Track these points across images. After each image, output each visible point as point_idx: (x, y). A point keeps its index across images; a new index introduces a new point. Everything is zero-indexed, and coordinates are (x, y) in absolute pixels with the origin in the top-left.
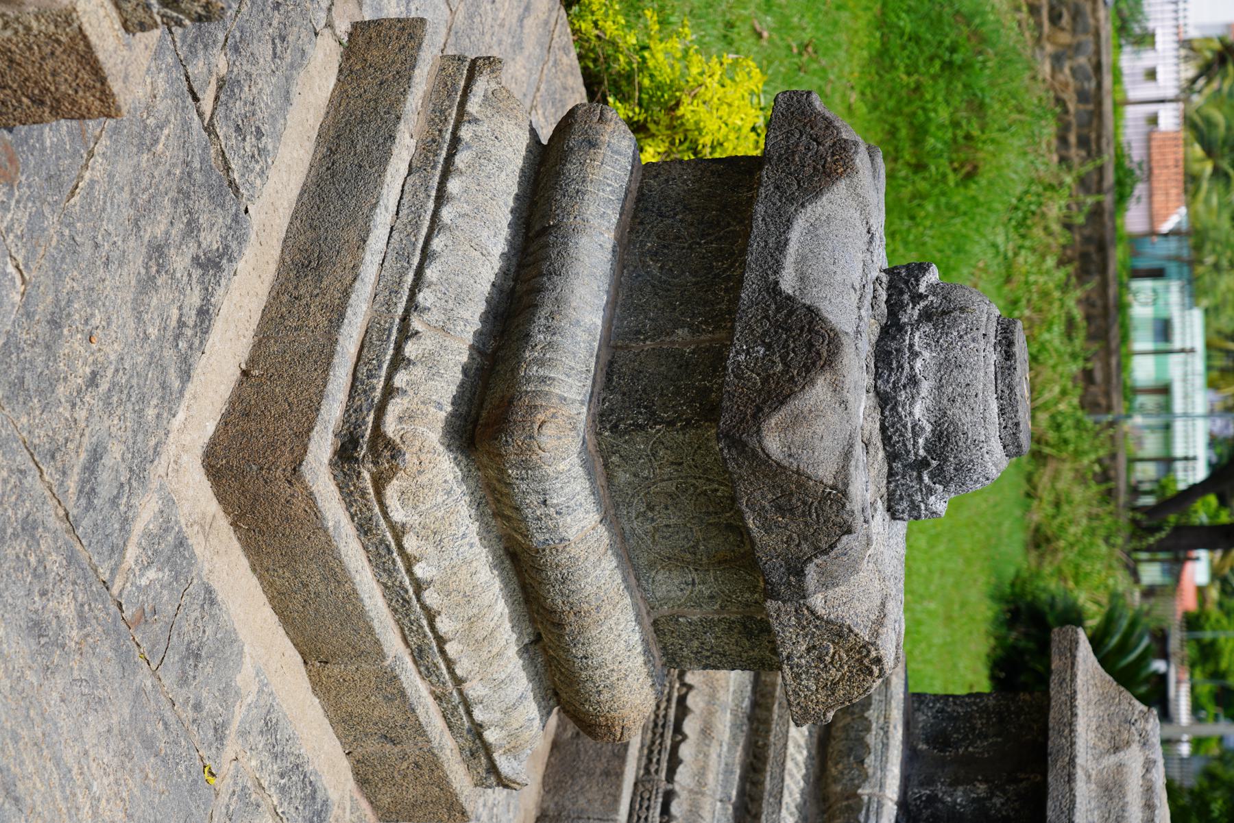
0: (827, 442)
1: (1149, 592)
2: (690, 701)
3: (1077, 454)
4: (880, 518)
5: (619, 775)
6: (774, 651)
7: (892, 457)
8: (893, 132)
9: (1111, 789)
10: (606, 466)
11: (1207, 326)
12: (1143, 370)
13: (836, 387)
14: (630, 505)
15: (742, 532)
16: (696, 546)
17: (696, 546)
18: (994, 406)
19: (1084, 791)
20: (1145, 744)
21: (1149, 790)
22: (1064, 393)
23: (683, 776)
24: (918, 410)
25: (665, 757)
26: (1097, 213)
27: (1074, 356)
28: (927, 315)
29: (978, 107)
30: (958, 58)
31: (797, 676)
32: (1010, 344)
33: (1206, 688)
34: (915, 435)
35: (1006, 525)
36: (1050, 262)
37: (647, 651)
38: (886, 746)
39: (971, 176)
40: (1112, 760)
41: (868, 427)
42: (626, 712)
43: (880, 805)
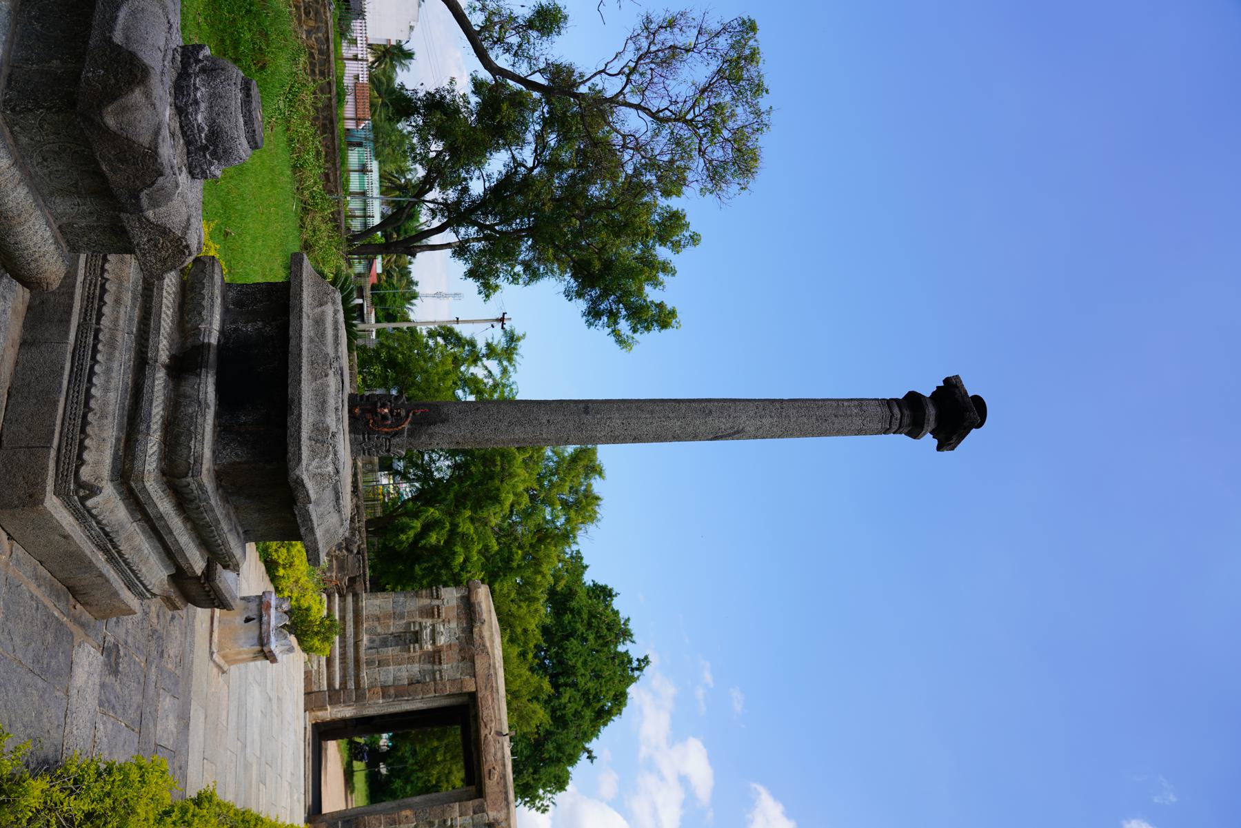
0: (144, 124)
1: (359, 275)
2: (107, 286)
3: (323, 210)
4: (183, 178)
5: (68, 321)
6: (131, 243)
7: (188, 143)
8: (222, 41)
9: (319, 322)
10: (12, 132)
11: (380, 169)
12: (355, 183)
13: (148, 95)
14: (31, 157)
15: (101, 175)
16: (76, 183)
17: (76, 183)
18: (241, 120)
19: (306, 323)
20: (334, 303)
21: (336, 322)
22: (315, 183)
23: (105, 322)
24: (200, 118)
25: (94, 313)
26: (328, 107)
27: (320, 167)
28: (203, 70)
29: (265, 35)
30: (254, 8)
31: (144, 255)
32: (249, 89)
33: (381, 314)
34: (200, 132)
35: (291, 238)
36: (308, 124)
37: (56, 242)
38: (212, 306)
39: (263, 68)
40: (318, 310)
41: (173, 125)
42: (48, 274)
43: (210, 332)
